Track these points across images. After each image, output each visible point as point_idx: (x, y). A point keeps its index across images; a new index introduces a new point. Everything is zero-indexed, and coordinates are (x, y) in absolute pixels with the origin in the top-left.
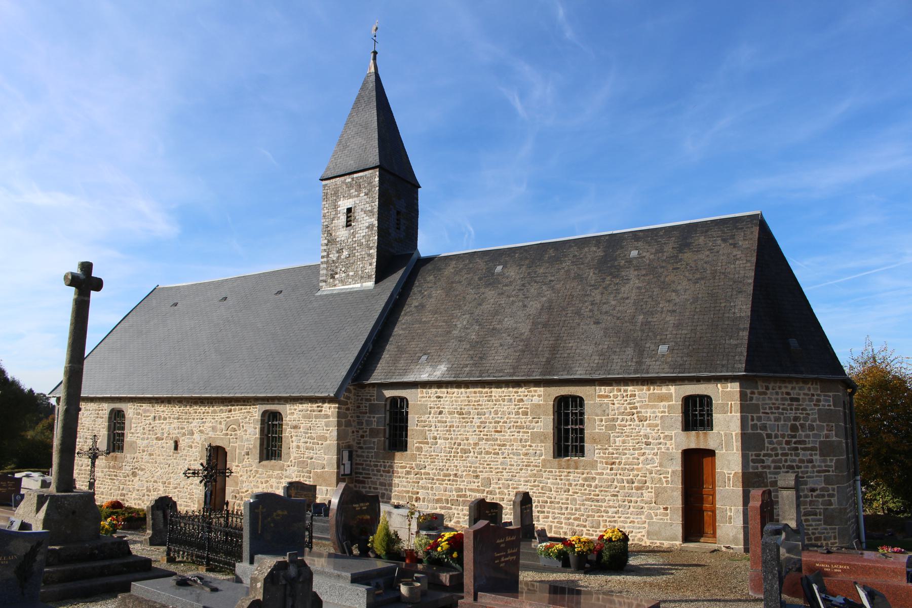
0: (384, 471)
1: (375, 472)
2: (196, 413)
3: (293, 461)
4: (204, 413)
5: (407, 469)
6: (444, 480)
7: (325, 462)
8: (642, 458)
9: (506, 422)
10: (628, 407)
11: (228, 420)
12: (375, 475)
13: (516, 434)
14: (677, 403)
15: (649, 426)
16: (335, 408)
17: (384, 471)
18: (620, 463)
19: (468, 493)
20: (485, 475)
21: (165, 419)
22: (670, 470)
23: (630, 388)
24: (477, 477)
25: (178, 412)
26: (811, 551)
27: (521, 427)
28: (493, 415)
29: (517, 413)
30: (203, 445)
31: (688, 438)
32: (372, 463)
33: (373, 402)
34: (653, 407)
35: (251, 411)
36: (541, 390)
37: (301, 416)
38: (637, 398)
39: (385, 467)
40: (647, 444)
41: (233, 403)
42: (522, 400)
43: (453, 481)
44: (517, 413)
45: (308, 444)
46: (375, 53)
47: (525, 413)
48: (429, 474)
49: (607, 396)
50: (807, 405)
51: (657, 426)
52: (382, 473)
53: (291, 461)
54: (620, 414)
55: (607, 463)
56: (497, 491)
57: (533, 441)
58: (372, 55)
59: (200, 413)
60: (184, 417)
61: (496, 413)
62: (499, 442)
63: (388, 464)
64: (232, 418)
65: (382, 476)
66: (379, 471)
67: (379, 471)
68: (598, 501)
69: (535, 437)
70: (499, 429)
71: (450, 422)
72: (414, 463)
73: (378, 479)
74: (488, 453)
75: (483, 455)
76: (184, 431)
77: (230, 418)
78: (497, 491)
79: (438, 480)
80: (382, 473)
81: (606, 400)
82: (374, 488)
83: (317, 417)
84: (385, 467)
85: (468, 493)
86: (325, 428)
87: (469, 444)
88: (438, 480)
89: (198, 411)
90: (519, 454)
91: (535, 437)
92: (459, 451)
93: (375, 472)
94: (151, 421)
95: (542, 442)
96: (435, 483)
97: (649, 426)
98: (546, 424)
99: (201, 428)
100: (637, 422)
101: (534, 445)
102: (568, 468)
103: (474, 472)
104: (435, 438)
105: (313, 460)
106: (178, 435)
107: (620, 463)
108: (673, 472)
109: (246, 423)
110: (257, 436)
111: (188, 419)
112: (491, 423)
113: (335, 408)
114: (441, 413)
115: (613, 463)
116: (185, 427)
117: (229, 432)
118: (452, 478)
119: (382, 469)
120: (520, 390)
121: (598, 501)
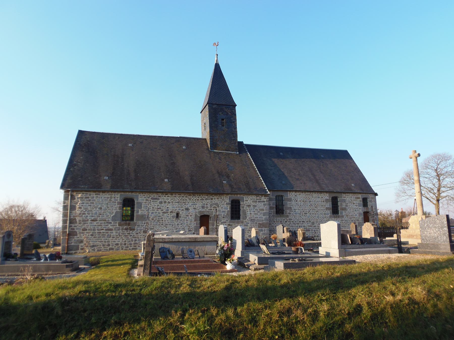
0: (276, 222)
1: (273, 222)
2: (190, 200)
3: (248, 219)
4: (195, 200)
5: (286, 220)
6: (299, 223)
7: (263, 219)
8: (354, 214)
9: (318, 204)
10: (350, 200)
11: (211, 203)
12: (273, 223)
13: (321, 208)
14: (361, 199)
15: (356, 205)
16: (267, 198)
17: (276, 222)
18: (349, 216)
19: (308, 227)
20: (313, 221)
21: (169, 203)
22: (361, 217)
23: (350, 195)
24: (310, 222)
25: (178, 200)
26: (101, 266)
27: (323, 206)
28: (314, 202)
29: (321, 201)
30: (196, 215)
31: (364, 208)
32: (271, 219)
33: (270, 197)
34: (356, 200)
35: (224, 199)
36: (328, 194)
37: (251, 202)
38: (352, 198)
39: (277, 220)
40: (355, 210)
41: (213, 196)
42: (322, 198)
43: (302, 223)
44: (321, 201)
45: (255, 212)
46: (217, 55)
47: (324, 202)
48: (293, 222)
49: (345, 197)
50: (163, 205)
51: (357, 205)
52: (276, 222)
53: (247, 219)
54: (349, 202)
55: (346, 216)
56: (317, 226)
57: (326, 210)
58: (216, 55)
59: (193, 200)
60: (182, 202)
61: (315, 201)
62: (316, 210)
63: (278, 219)
64: (213, 202)
65: (276, 223)
66: (274, 222)
67: (274, 222)
68: (345, 227)
69: (327, 209)
70: (316, 206)
71: (300, 204)
72: (288, 218)
73: (274, 225)
74: (313, 214)
75: (312, 215)
76: (183, 208)
77: (212, 202)
78: (317, 226)
79: (297, 223)
80: (276, 222)
81: (345, 198)
82: (273, 228)
83: (259, 202)
84: (277, 220)
85: (308, 227)
86: (263, 206)
87: (307, 211)
88: (297, 223)
89: (191, 199)
90: (322, 214)
91: (327, 209)
92: (304, 213)
93: (273, 222)
94: (158, 204)
95: (329, 210)
96: (296, 225)
97: (356, 205)
98: (329, 205)
99: (194, 207)
100: (352, 204)
101: (327, 211)
102: (337, 218)
103: (309, 220)
104: (295, 209)
105: (258, 218)
106: (179, 211)
107: (349, 216)
108: (362, 218)
109: (222, 204)
110: (229, 210)
111: (185, 203)
112: (313, 204)
113: (267, 198)
114: (297, 201)
115: (348, 216)
116: (184, 206)
117: (212, 208)
118: (302, 222)
119: (276, 221)
120: (322, 194)
121: (345, 227)
